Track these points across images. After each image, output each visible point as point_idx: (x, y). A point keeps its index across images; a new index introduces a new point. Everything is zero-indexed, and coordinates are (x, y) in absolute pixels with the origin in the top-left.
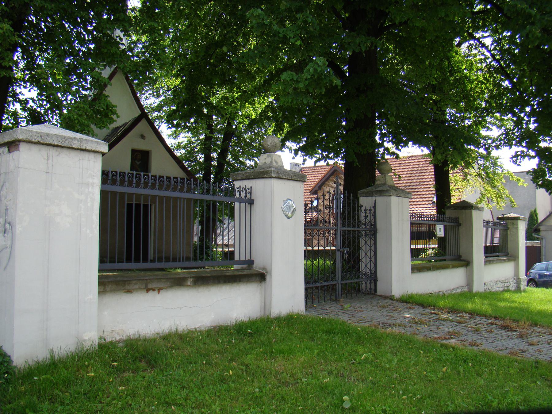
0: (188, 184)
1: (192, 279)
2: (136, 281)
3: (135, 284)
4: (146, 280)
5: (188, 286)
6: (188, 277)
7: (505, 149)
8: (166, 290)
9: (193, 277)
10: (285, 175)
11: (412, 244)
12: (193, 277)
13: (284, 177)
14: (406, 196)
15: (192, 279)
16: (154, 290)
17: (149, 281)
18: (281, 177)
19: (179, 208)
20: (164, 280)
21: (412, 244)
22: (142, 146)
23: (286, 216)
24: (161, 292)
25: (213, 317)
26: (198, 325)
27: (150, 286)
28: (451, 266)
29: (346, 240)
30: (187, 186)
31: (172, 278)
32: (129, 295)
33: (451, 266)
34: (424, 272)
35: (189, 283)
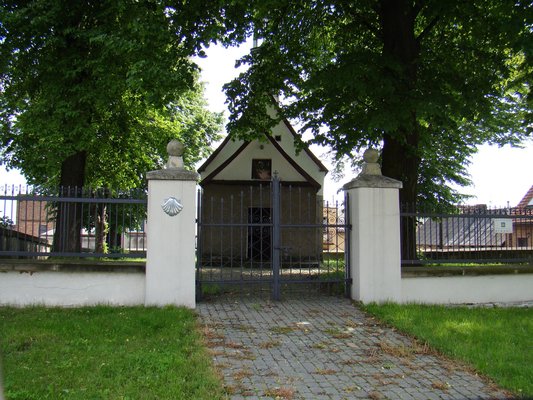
0: (72, 190)
1: (57, 266)
2: (4, 264)
3: (3, 266)
4: (13, 263)
5: (53, 271)
6: (54, 264)
7: (16, 118)
8: (38, 273)
9: (59, 264)
10: (164, 176)
11: (145, 263)
12: (59, 264)
13: (163, 178)
14: (391, 186)
15: (57, 266)
16: (27, 272)
17: (15, 264)
18: (159, 177)
19: (68, 208)
20: (30, 265)
21: (145, 263)
22: (261, 155)
23: (167, 213)
24: (34, 274)
25: (87, 299)
26: (71, 304)
27: (16, 268)
28: (516, 271)
29: (260, 237)
30: (71, 192)
31: (38, 264)
32: (4, 274)
33: (516, 271)
34: (456, 276)
35: (55, 269)
